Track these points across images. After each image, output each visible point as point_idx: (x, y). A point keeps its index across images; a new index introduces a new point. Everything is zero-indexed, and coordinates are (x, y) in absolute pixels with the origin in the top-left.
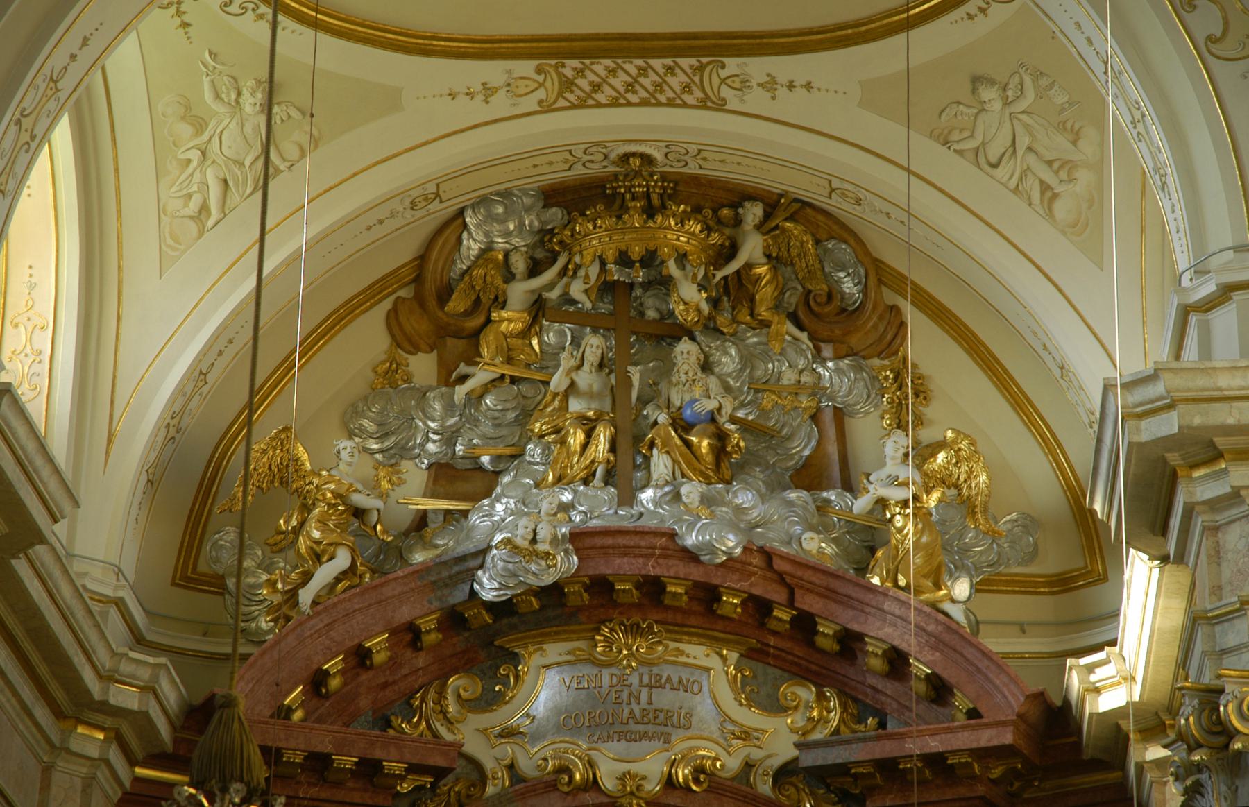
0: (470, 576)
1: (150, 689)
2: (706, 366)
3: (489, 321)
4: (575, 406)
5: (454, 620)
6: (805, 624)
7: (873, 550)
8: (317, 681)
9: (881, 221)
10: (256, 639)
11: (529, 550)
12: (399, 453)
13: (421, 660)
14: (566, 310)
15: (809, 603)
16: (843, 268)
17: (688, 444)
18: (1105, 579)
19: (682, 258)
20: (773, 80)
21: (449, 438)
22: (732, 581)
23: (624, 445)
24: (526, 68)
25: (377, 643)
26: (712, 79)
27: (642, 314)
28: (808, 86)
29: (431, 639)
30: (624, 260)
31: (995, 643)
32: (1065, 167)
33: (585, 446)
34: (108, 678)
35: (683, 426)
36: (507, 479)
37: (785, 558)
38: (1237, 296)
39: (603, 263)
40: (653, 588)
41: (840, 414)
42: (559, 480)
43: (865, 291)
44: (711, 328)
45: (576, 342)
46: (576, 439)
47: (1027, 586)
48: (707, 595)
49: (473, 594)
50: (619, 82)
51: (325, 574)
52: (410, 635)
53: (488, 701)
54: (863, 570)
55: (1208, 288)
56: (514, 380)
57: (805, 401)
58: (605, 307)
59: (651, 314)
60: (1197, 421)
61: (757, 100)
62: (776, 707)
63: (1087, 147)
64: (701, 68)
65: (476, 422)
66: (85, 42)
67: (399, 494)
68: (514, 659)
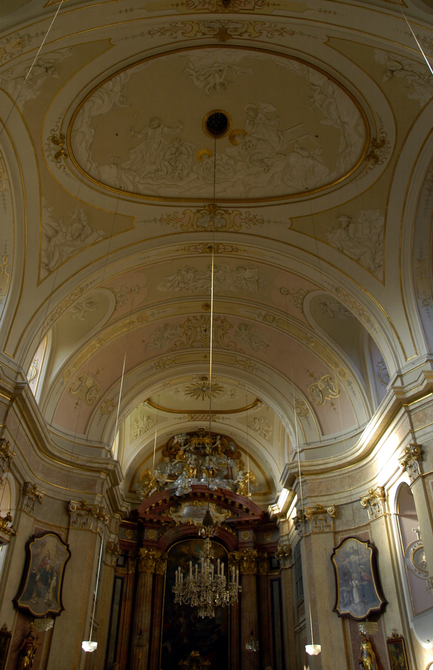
0: (175, 492)
1: (127, 508)
2: (211, 460)
3: (177, 453)
4: (191, 466)
5: (171, 499)
6: (226, 500)
10: (140, 501)
11: (184, 488)
12: (162, 473)
13: (166, 505)
14: (189, 451)
15: (227, 497)
16: (232, 446)
18: (271, 493)
19: (208, 444)
21: (171, 471)
23: (199, 472)
24: (186, 415)
25: (160, 502)
27: (201, 452)
29: (168, 501)
30: (199, 444)
31: (257, 503)
32: (267, 431)
33: (193, 472)
34: (121, 506)
35: (208, 469)
36: (180, 477)
37: (224, 490)
38: (304, 451)
39: (195, 444)
40: (203, 494)
41: (231, 468)
42: (188, 477)
43: (235, 449)
44: (212, 455)
45: (191, 456)
46: (191, 471)
47: (259, 494)
48: (211, 495)
49: (175, 495)
50: (200, 417)
51: (153, 491)
52: (165, 501)
53: (176, 511)
56: (181, 462)
57: (226, 466)
58: (195, 451)
59: (202, 452)
61: (221, 421)
62: (221, 513)
63: (271, 429)
64: (213, 416)
66: (129, 410)
68: (180, 505)
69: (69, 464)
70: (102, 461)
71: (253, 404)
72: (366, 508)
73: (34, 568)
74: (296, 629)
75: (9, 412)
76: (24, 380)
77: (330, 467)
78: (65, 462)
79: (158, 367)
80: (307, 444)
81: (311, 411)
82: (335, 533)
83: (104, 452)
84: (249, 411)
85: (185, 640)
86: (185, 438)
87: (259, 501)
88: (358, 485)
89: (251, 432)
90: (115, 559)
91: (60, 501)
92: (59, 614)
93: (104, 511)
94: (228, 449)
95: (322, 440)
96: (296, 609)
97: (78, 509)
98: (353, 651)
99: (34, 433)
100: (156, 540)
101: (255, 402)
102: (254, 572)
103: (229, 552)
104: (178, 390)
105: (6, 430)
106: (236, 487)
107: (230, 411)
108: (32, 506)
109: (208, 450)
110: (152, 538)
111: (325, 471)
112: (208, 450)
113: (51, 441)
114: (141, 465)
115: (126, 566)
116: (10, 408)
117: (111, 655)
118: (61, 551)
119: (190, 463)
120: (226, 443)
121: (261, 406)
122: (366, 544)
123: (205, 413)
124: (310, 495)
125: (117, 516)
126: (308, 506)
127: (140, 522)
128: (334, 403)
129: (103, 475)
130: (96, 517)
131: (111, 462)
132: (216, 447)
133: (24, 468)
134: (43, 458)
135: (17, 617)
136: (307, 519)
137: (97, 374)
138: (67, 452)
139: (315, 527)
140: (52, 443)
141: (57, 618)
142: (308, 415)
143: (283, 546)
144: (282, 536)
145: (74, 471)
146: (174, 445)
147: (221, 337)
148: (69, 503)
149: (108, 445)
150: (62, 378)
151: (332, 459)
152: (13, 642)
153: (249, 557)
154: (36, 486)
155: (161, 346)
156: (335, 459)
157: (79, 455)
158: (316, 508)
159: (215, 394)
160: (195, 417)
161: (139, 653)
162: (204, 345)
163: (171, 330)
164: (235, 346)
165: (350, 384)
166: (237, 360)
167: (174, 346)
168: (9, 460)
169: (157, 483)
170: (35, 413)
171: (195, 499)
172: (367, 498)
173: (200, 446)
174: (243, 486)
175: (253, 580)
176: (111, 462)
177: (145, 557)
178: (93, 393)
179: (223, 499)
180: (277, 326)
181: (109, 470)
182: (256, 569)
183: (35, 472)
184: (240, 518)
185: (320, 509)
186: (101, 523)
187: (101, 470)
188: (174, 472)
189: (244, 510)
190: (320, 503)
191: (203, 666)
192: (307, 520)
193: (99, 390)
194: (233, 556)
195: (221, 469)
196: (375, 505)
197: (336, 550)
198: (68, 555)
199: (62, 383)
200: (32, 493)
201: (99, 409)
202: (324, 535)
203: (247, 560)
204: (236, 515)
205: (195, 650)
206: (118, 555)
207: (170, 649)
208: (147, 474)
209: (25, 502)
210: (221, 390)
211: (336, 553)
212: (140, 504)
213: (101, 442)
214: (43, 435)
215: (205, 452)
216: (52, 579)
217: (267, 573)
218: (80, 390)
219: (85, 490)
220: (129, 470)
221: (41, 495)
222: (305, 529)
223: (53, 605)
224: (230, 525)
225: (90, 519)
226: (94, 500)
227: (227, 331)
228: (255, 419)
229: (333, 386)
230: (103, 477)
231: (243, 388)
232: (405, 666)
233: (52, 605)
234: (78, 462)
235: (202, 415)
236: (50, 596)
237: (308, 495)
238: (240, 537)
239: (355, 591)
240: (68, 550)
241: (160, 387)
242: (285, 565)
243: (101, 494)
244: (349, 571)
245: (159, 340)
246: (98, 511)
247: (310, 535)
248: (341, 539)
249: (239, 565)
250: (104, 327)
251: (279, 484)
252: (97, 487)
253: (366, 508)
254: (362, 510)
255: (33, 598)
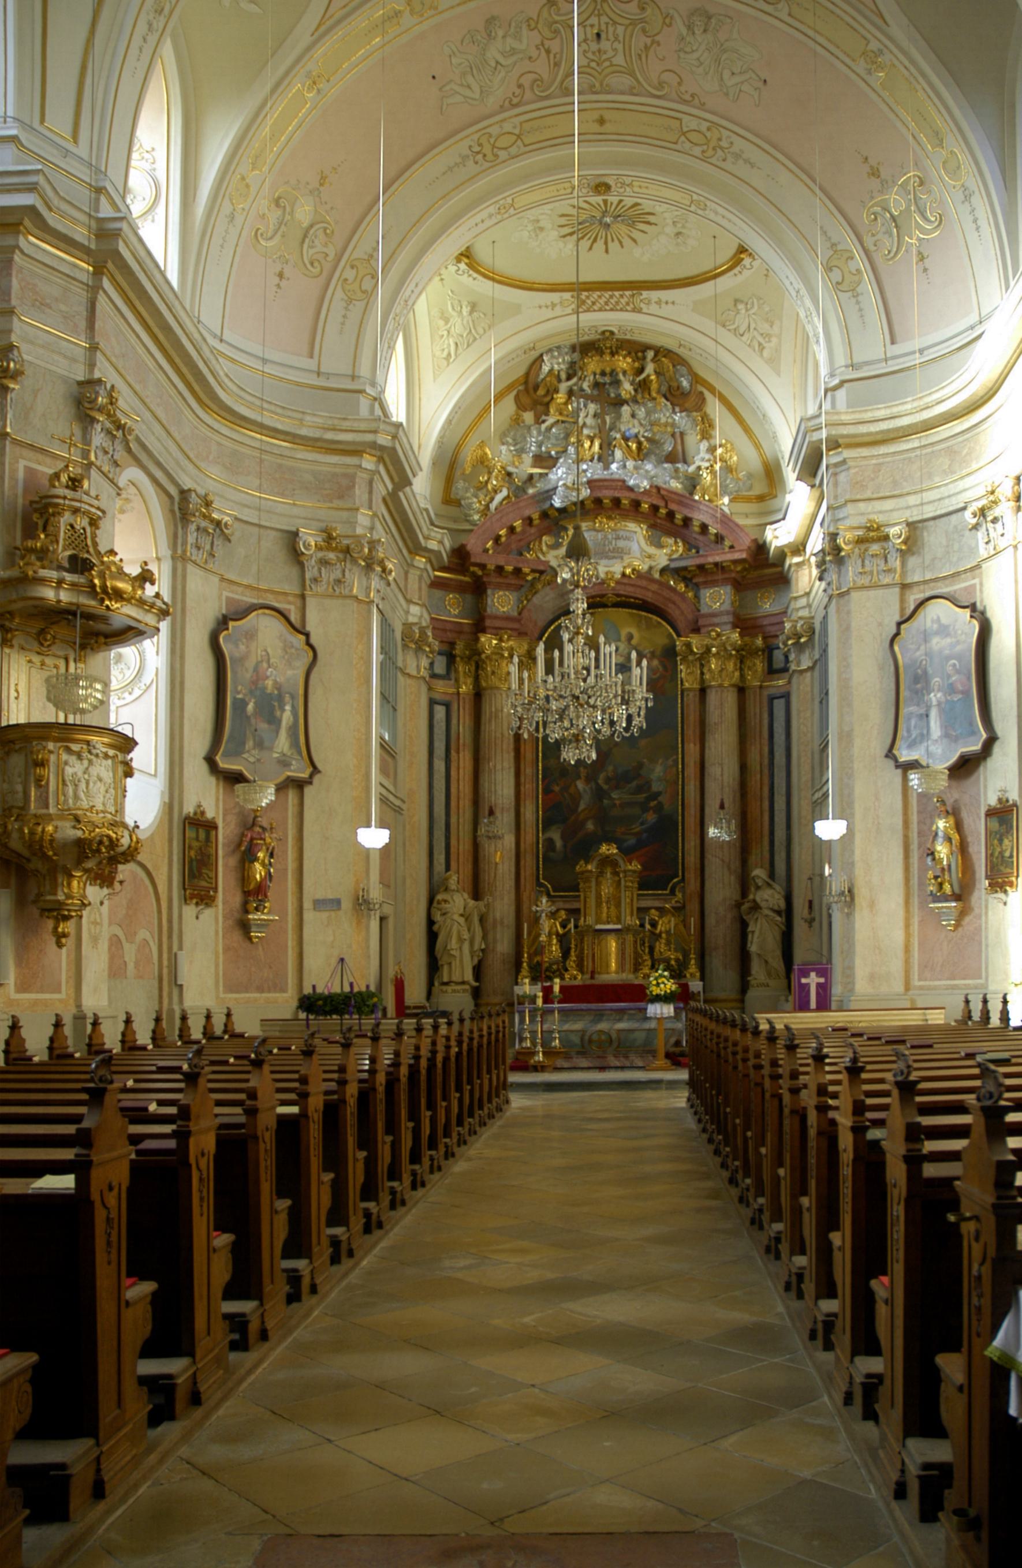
0: (551, 498)
1: (441, 542)
2: (633, 416)
3: (552, 398)
4: (586, 432)
5: (544, 515)
6: (671, 515)
7: (695, 487)
8: (497, 539)
9: (698, 358)
12: (520, 452)
13: (533, 530)
15: (673, 506)
16: (683, 376)
17: (628, 446)
18: (776, 497)
19: (625, 373)
20: (660, 301)
21: (540, 446)
22: (645, 499)
23: (605, 446)
24: (567, 295)
25: (518, 524)
26: (637, 300)
27: (609, 395)
28: (673, 303)
29: (536, 522)
30: (603, 374)
31: (741, 521)
32: (768, 336)
33: (590, 447)
35: (626, 439)
36: (561, 460)
38: (846, 385)
39: (595, 374)
41: (682, 434)
43: (691, 386)
44: (635, 401)
45: (585, 406)
46: (587, 444)
47: (748, 500)
48: (636, 504)
49: (552, 505)
50: (602, 301)
51: (499, 498)
52: (529, 521)
54: (692, 494)
55: (836, 381)
56: (563, 422)
57: (669, 429)
58: (595, 392)
59: (612, 395)
60: (834, 432)
61: (654, 309)
62: (660, 546)
63: (776, 328)
64: (633, 295)
65: (549, 438)
66: (417, 285)
67: (523, 467)
69: (282, 437)
70: (363, 426)
71: (731, 259)
72: (976, 527)
73: (239, 688)
74: (816, 796)
75: (98, 305)
76: (119, 210)
77: (902, 427)
78: (272, 434)
79: (480, 157)
80: (853, 366)
81: (867, 277)
82: (905, 587)
83: (364, 403)
84: (719, 280)
85: (590, 826)
86: (567, 358)
87: (747, 516)
88: (964, 472)
89: (726, 337)
90: (424, 662)
91: (274, 533)
92: (309, 782)
93: (380, 549)
94: (674, 384)
95: (888, 355)
96: (817, 756)
97: (319, 548)
98: (919, 833)
99: (177, 360)
100: (515, 614)
101: (735, 255)
102: (734, 681)
103: (679, 635)
104: (541, 224)
105: (98, 354)
106: (693, 482)
107: (675, 280)
108: (208, 547)
109: (627, 388)
110: (505, 609)
111: (892, 436)
112: (627, 388)
113: (226, 380)
114: (466, 435)
115: (453, 675)
116: (97, 293)
117: (440, 858)
118: (292, 647)
119: (584, 424)
120: (668, 371)
121: (752, 267)
122: (967, 612)
123: (612, 290)
124: (854, 497)
125: (421, 561)
126: (848, 523)
127: (474, 574)
128: (925, 255)
129: (368, 462)
130: (363, 564)
131: (382, 426)
132: (644, 380)
133: (170, 454)
134: (216, 426)
135: (221, 791)
136: (843, 554)
137: (321, 185)
138: (273, 408)
139: (861, 573)
140: (230, 384)
141: (308, 791)
142: (859, 289)
143: (797, 621)
144: (796, 598)
145: (299, 456)
146: (543, 380)
147: (640, 56)
148: (296, 534)
149: (373, 384)
150: (227, 200)
151: (908, 406)
152: (224, 838)
153: (723, 646)
154: (211, 498)
155: (482, 92)
156: (915, 404)
157: (303, 413)
158: (866, 527)
159: (636, 234)
160: (589, 302)
161: (496, 852)
162: (597, 85)
163: (504, 37)
164: (680, 84)
165: (967, 197)
166: (685, 129)
167: (518, 91)
168: (124, 435)
169: (507, 478)
170: (167, 304)
171: (598, 515)
172: (980, 504)
173: (607, 379)
174: (709, 478)
175: (731, 699)
176: (382, 426)
177: (492, 653)
178: (316, 242)
179: (663, 511)
180: (790, 15)
181: (382, 448)
182: (737, 674)
183: (202, 465)
184: (702, 556)
185: (873, 531)
186: (377, 579)
187: (360, 448)
188: (547, 447)
189: (713, 538)
190: (875, 517)
191: (625, 872)
192: (843, 557)
193: (333, 232)
194: (688, 645)
195: (657, 438)
196: (995, 521)
197: (903, 626)
198: (311, 654)
199: (232, 218)
200: (204, 516)
201: (339, 287)
202: (880, 592)
203: (718, 653)
204: (694, 551)
205: (609, 840)
206: (431, 652)
207: (559, 843)
208: (482, 457)
209: (191, 539)
210: (649, 223)
211: (902, 632)
212: (471, 531)
213: (353, 377)
214: (201, 365)
215: (620, 395)
216: (283, 710)
217: (763, 682)
218: (283, 236)
219: (331, 502)
220: (440, 447)
221: (226, 518)
222: (839, 577)
223: (294, 762)
224: (681, 573)
225: (350, 570)
226: (353, 524)
227: (657, 38)
228: (736, 301)
229: (925, 204)
230: (369, 468)
231: (700, 212)
232: (1011, 856)
233: (290, 764)
234: (304, 432)
235: (607, 294)
236: (282, 743)
237: (848, 497)
238: (702, 601)
239: (934, 713)
240: (308, 644)
241: (490, 216)
242: (798, 664)
243: (370, 508)
244: (925, 672)
245: (475, 71)
246: (366, 550)
247: (848, 592)
248: (915, 600)
249: (702, 666)
250: (316, 35)
251: (790, 475)
252: (357, 492)
253: (976, 527)
254: (967, 533)
255: (248, 752)
